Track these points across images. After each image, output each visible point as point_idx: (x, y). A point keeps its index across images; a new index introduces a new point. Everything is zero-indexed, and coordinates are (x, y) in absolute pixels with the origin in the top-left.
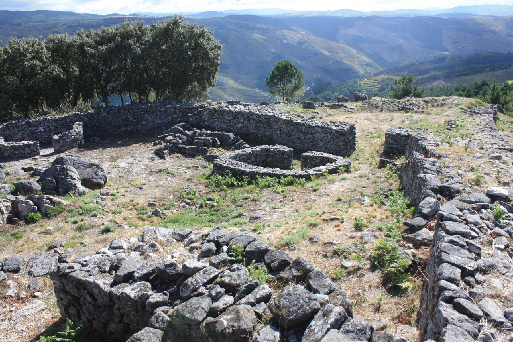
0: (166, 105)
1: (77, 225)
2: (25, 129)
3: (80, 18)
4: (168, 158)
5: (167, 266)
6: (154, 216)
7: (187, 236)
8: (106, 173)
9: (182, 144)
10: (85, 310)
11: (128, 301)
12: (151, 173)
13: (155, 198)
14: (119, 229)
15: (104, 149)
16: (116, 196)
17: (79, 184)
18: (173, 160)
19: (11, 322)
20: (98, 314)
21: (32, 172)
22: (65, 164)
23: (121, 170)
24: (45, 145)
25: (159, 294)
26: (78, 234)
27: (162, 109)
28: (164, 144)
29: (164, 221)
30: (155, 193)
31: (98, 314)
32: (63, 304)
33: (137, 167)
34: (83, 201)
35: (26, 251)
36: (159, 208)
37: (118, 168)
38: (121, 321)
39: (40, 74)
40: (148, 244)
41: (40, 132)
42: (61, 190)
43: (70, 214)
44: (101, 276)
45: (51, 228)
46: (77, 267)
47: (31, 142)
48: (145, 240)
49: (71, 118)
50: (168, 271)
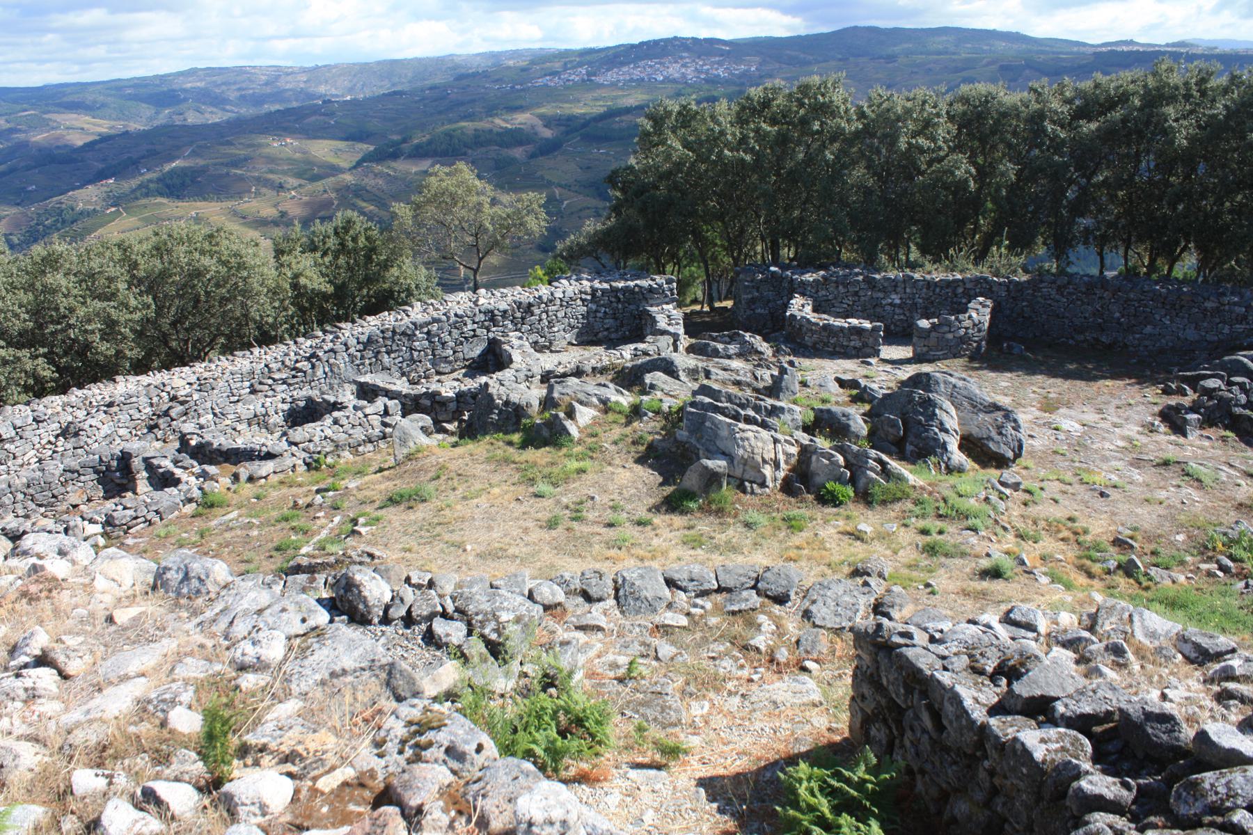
0: (1223, 294)
1: (928, 539)
2: (861, 293)
3: (1035, 48)
4: (1194, 435)
5: (1149, 716)
6: (1120, 572)
7: (1219, 656)
8: (1022, 435)
9: (1244, 407)
10: (907, 743)
11: (1023, 765)
12: (1137, 463)
13: (1135, 529)
14: (1024, 579)
15: (1028, 374)
16: (1036, 498)
17: (953, 444)
18: (1206, 443)
19: (747, 703)
20: (937, 764)
21: (855, 392)
22: (931, 391)
23: (1062, 436)
24: (895, 337)
25: (1110, 779)
26: (925, 561)
27: (1209, 305)
28: (1191, 397)
29: (1145, 594)
30: (1137, 515)
31: (937, 764)
32: (862, 709)
33: (1104, 438)
34: (954, 487)
35: (803, 564)
36: (1139, 557)
37: (1056, 429)
38: (987, 804)
39: (923, 173)
40: (1105, 643)
41: (891, 304)
42: (909, 448)
43: (917, 510)
44: (971, 678)
45: (869, 529)
46: (920, 638)
47: (867, 325)
48: (1098, 628)
49: (968, 286)
50: (1150, 731)
